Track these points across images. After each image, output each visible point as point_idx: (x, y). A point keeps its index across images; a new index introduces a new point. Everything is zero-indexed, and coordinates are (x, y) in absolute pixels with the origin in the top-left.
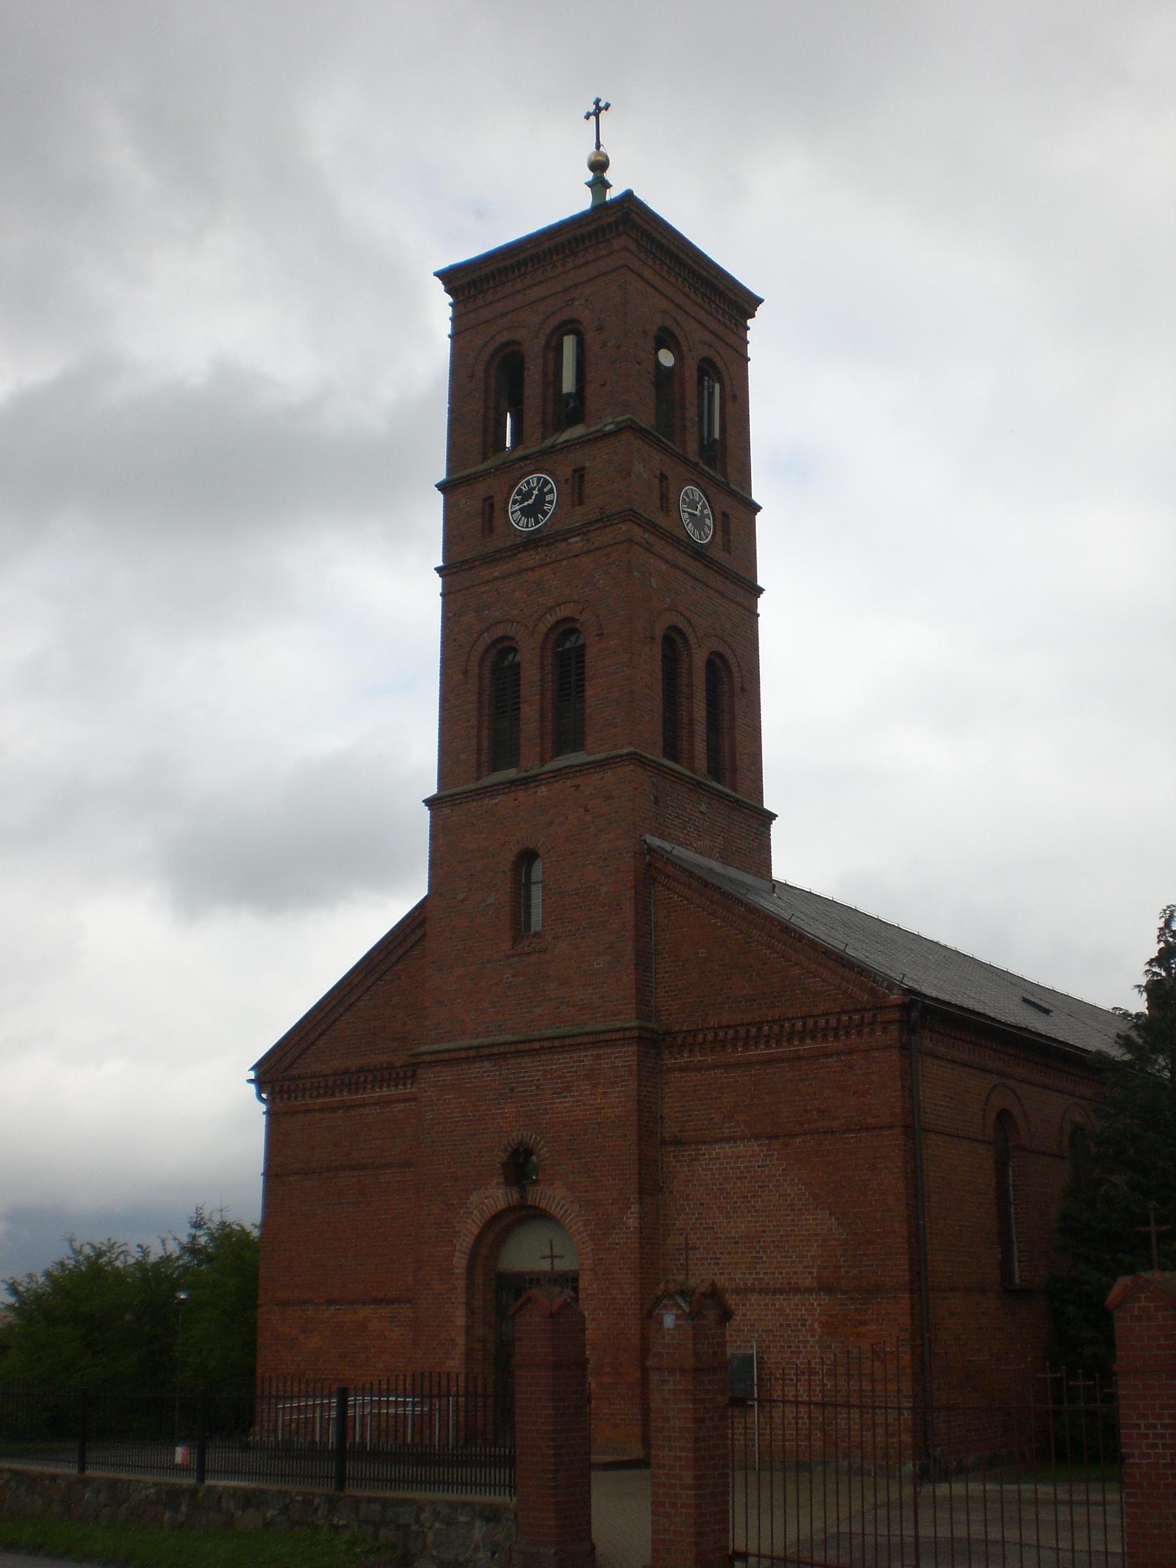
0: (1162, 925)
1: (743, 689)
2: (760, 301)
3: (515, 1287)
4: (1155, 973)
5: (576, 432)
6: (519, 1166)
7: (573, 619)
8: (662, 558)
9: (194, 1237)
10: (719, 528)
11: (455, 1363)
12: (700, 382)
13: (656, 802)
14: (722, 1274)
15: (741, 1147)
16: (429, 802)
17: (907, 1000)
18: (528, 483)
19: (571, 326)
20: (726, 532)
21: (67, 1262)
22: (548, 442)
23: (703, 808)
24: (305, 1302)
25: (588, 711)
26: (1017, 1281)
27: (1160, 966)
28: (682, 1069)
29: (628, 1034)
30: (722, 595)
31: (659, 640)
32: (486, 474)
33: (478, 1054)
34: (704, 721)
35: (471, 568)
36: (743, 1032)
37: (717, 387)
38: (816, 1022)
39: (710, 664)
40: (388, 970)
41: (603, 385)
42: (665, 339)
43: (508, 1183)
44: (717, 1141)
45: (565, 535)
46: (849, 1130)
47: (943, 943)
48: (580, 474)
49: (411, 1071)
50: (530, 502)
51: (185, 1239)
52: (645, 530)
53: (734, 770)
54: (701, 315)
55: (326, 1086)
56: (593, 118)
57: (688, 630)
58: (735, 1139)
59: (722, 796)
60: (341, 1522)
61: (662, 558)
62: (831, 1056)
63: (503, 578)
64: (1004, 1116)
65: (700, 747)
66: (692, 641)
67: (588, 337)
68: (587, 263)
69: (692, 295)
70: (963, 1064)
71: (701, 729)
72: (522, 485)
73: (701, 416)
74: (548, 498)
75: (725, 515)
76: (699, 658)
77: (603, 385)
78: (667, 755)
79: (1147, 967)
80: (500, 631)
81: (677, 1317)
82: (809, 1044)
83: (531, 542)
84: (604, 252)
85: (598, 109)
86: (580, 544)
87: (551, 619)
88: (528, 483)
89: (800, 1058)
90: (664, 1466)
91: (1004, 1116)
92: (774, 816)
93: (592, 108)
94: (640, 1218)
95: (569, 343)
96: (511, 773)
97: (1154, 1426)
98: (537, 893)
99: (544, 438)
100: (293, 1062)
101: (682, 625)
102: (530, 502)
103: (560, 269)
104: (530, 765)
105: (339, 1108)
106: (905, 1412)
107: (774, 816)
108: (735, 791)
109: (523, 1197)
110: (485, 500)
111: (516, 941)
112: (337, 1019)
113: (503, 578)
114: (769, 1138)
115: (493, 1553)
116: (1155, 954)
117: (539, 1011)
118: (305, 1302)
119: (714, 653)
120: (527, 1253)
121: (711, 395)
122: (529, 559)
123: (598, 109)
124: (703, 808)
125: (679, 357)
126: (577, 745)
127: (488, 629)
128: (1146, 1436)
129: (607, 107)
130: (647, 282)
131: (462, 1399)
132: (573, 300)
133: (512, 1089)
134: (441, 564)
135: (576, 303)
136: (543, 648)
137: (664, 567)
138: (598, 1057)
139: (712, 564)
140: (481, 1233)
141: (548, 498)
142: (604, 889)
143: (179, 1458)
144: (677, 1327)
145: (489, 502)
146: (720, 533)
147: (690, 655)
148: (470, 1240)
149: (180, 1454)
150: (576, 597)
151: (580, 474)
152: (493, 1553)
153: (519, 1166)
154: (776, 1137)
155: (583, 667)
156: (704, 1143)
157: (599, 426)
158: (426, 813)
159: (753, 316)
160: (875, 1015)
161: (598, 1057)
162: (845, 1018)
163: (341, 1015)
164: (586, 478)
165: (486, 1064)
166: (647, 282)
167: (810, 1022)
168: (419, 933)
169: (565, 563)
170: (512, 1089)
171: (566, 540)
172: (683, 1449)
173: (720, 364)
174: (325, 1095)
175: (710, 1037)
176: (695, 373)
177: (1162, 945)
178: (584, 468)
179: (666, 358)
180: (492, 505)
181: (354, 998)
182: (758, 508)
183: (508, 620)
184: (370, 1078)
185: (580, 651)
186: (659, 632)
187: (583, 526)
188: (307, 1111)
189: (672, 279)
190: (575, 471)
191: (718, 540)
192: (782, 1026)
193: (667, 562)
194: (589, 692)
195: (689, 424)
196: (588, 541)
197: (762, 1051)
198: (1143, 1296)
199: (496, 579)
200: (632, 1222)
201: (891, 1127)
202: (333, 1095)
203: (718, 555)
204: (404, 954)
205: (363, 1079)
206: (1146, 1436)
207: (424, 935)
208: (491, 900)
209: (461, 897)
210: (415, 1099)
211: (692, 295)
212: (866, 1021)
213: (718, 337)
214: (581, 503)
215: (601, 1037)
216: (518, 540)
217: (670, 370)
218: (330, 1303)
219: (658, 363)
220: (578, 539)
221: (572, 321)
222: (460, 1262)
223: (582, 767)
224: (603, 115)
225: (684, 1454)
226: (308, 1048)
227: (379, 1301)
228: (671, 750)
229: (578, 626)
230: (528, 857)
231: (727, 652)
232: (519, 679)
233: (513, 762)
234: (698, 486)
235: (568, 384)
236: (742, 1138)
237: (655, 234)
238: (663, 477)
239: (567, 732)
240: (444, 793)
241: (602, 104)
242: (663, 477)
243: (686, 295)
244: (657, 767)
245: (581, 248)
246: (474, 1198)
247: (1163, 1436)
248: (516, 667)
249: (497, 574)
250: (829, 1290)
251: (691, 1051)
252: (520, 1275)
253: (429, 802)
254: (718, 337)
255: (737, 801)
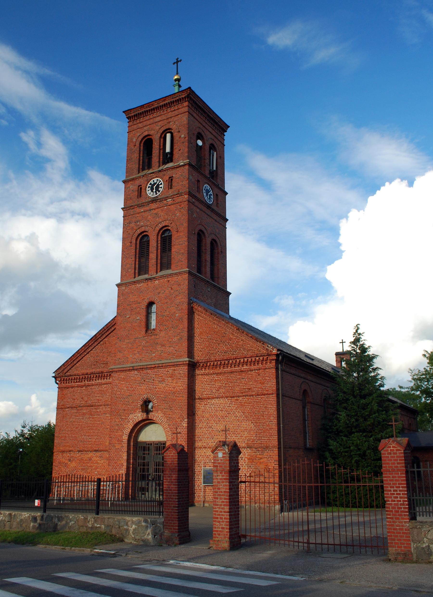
0: (355, 332)
1: (222, 252)
2: (229, 127)
3: (146, 447)
4: (352, 347)
5: (170, 165)
6: (145, 406)
7: (168, 226)
8: (198, 208)
9: (23, 431)
10: (215, 199)
11: (123, 471)
12: (210, 152)
13: (195, 287)
14: (214, 442)
15: (222, 400)
16: (118, 285)
17: (279, 352)
18: (154, 181)
19: (168, 130)
20: (217, 200)
21: (427, 368)
22: (160, 168)
23: (209, 290)
24: (70, 451)
25: (172, 256)
26: (308, 446)
27: (354, 345)
28: (202, 375)
29: (185, 363)
30: (216, 221)
31: (196, 234)
32: (140, 177)
33: (133, 369)
34: (209, 261)
35: (133, 208)
36: (223, 362)
37: (215, 153)
38: (248, 360)
39: (211, 243)
40: (102, 340)
41: (180, 150)
42: (200, 136)
43: (143, 411)
44: (213, 398)
45: (166, 199)
46: (258, 395)
47: (277, 338)
48: (171, 179)
49: (110, 374)
50: (154, 187)
51: (19, 431)
52: (193, 198)
53: (218, 278)
54: (210, 130)
55: (80, 379)
56: (176, 64)
57: (205, 231)
58: (219, 398)
59: (215, 286)
60: (98, 526)
61: (198, 208)
62: (252, 370)
63: (144, 212)
64: (305, 392)
65: (208, 270)
66: (207, 235)
67: (175, 134)
68: (175, 110)
69: (208, 123)
70: (294, 374)
71: (208, 264)
72: (151, 181)
73: (210, 162)
74: (160, 186)
75: (217, 195)
76: (208, 241)
77: (180, 150)
78: (198, 272)
79: (350, 344)
80: (143, 229)
81: (223, 454)
82: (245, 367)
83: (154, 200)
84: (180, 107)
85: (177, 62)
86: (171, 202)
87: (160, 226)
88: (154, 181)
89: (242, 371)
90: (218, 505)
91: (305, 392)
92: (230, 293)
93: (176, 61)
94: (188, 423)
95: (168, 136)
96: (146, 276)
97: (396, 491)
98: (154, 317)
99: (159, 166)
100: (68, 371)
101: (203, 229)
102: (154, 187)
103: (166, 112)
104: (152, 273)
105: (84, 386)
106: (276, 488)
107: (230, 293)
108: (218, 284)
109: (147, 417)
110: (139, 186)
111: (146, 331)
112: (84, 357)
113: (144, 212)
114: (231, 397)
115: (155, 536)
116: (353, 340)
117: (154, 355)
118: (70, 451)
119: (213, 239)
120: (152, 434)
121: (213, 156)
122: (154, 206)
123: (177, 62)
124: (209, 290)
125: (204, 143)
126: (168, 266)
127: (139, 228)
128: (394, 494)
129: (181, 61)
130: (194, 118)
131: (124, 483)
132: (170, 122)
133: (144, 380)
134: (123, 207)
135: (171, 123)
136: (158, 235)
137: (198, 210)
138: (174, 370)
139: (213, 210)
140: (133, 427)
141: (160, 186)
142: (177, 315)
143: (36, 504)
144: (223, 457)
145: (171, 187)
146: (215, 200)
147: (205, 240)
148: (129, 430)
149: (37, 502)
150: (169, 219)
151: (171, 179)
152: (155, 536)
153: (145, 406)
154: (234, 397)
155: (171, 242)
156: (209, 399)
157: (178, 164)
158: (117, 288)
159: (226, 132)
160: (267, 358)
161: (174, 370)
162: (257, 358)
163: (85, 355)
164: (173, 180)
165: (136, 372)
166: (194, 118)
167: (246, 360)
168: (113, 328)
169: (166, 207)
170: (144, 380)
171: (166, 200)
172: (225, 499)
173: (216, 146)
174: (79, 382)
175: (212, 364)
176: (208, 148)
177: (355, 338)
178: (173, 177)
179: (200, 143)
180: (141, 188)
181: (90, 350)
182: (227, 194)
183: (146, 226)
184: (95, 376)
185: (170, 237)
186: (197, 231)
187: (172, 196)
188: (72, 387)
189: (202, 117)
190: (170, 178)
191: (214, 203)
192: (236, 361)
193: (199, 208)
194: (173, 250)
195: (206, 165)
196: (174, 200)
197: (229, 369)
198: (391, 446)
199: (142, 212)
200: (185, 425)
201: (272, 394)
202: (82, 382)
203: (215, 208)
204: (108, 335)
205: (92, 376)
206: (394, 494)
207: (115, 329)
208: (138, 318)
209: (128, 317)
210: (110, 383)
211: (208, 123)
212: (264, 359)
213: (215, 137)
214: (171, 188)
215: (175, 364)
216: (150, 200)
217: (201, 147)
218: (79, 451)
219: (197, 145)
220: (170, 200)
221: (169, 129)
222: (125, 438)
223: (171, 275)
224: (179, 63)
225: (225, 500)
226: (73, 366)
227: (96, 451)
228: (199, 270)
229: (170, 228)
230: (151, 304)
231: (217, 240)
232: (149, 245)
233: (146, 272)
234: (209, 185)
235: (168, 150)
236: (222, 397)
237: (197, 102)
238: (198, 181)
239: (165, 263)
240: (124, 282)
241: (179, 60)
242: (198, 181)
243: (206, 123)
244: (195, 275)
245: (173, 105)
246: (131, 416)
247: (400, 494)
248: (148, 242)
249: (142, 210)
250: (250, 447)
251: (205, 369)
252: (145, 442)
253: (118, 285)
254: (215, 137)
255: (219, 288)
